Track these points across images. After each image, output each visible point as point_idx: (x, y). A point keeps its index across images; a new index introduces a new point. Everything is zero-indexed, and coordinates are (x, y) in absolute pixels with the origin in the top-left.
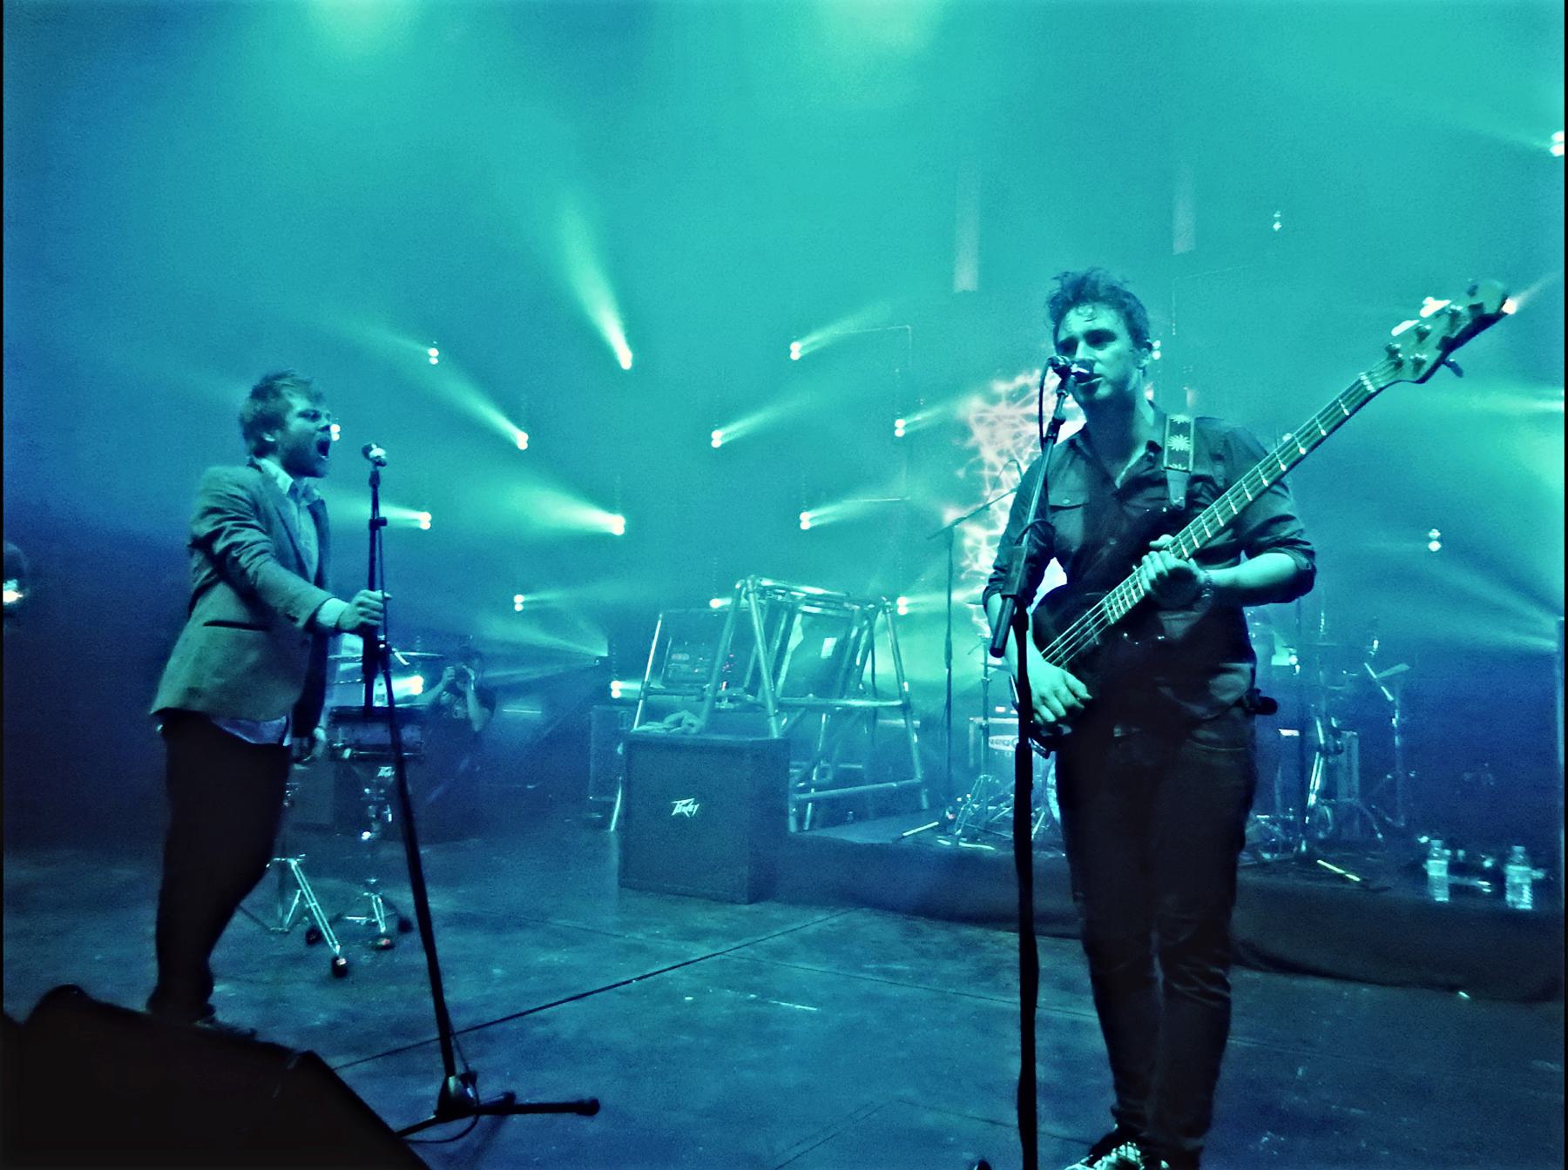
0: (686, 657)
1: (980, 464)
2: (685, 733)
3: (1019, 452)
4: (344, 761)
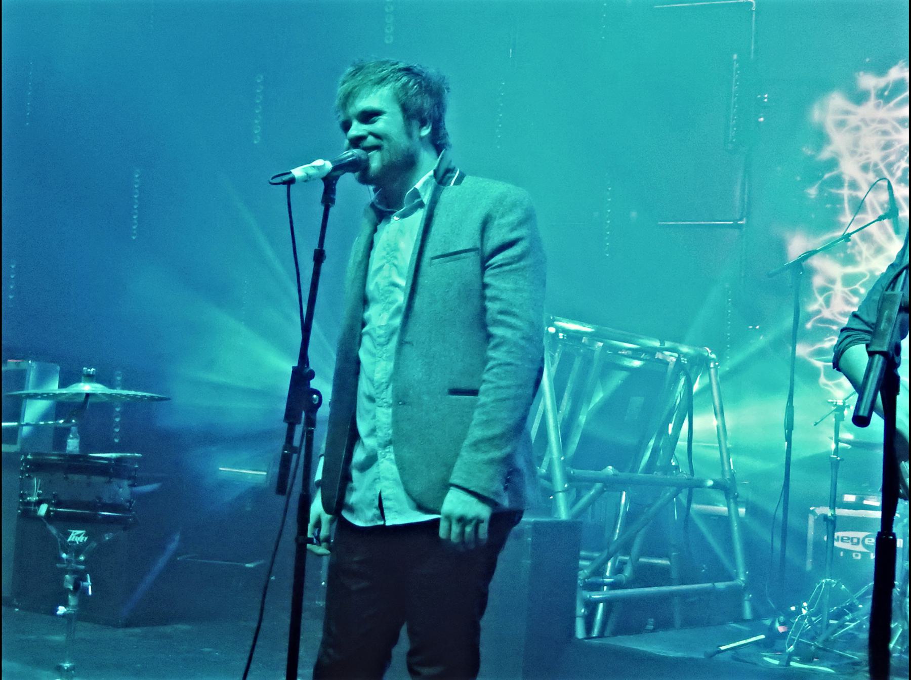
1: (838, 181)
3: (890, 166)
4: (39, 518)
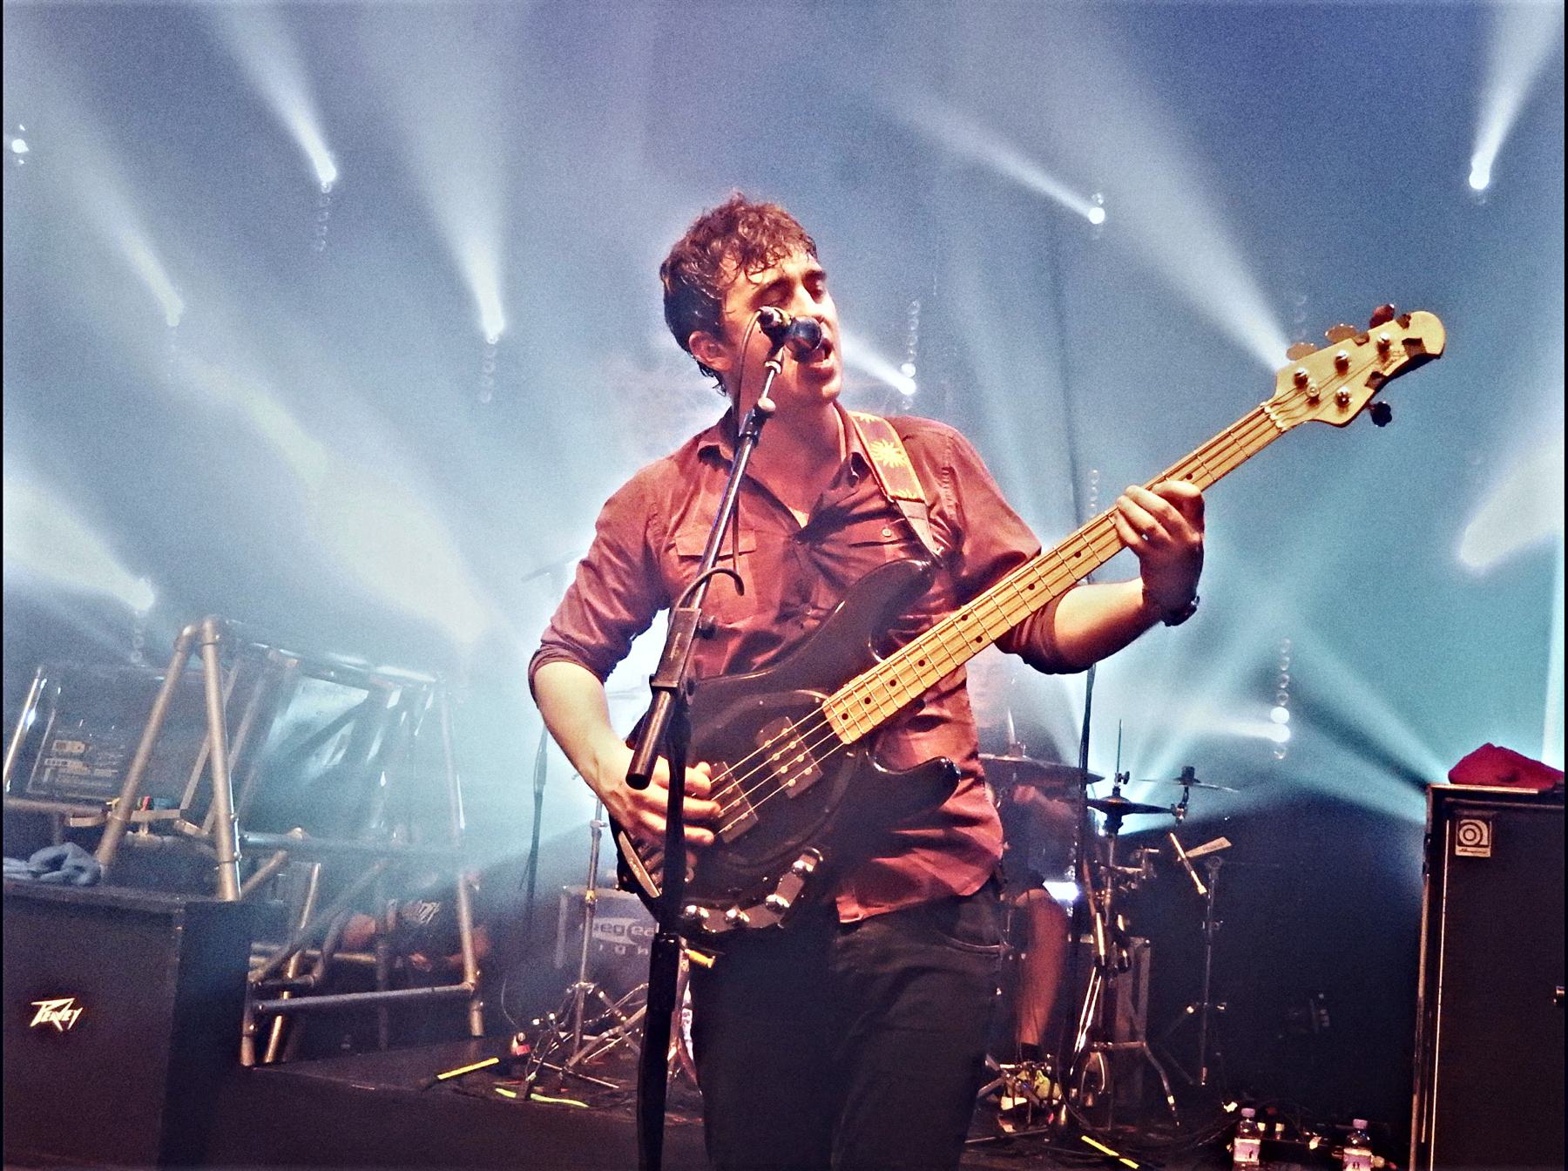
0: (77, 747)
2: (67, 881)
